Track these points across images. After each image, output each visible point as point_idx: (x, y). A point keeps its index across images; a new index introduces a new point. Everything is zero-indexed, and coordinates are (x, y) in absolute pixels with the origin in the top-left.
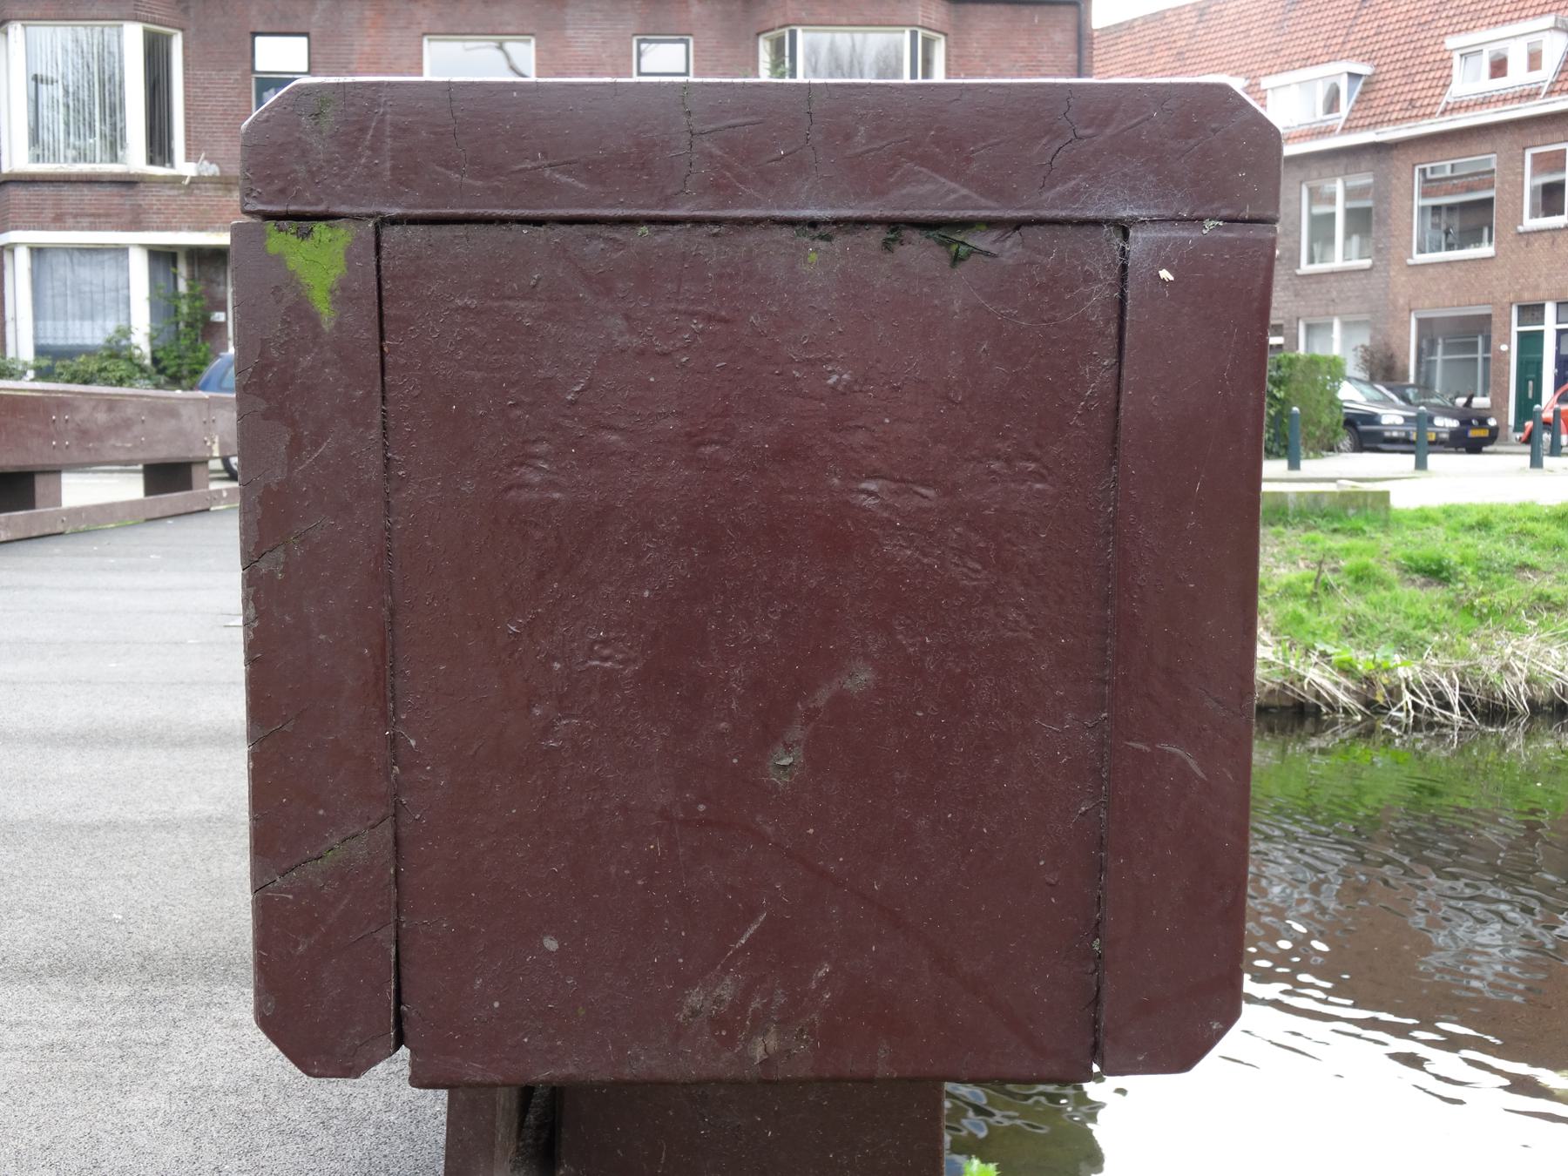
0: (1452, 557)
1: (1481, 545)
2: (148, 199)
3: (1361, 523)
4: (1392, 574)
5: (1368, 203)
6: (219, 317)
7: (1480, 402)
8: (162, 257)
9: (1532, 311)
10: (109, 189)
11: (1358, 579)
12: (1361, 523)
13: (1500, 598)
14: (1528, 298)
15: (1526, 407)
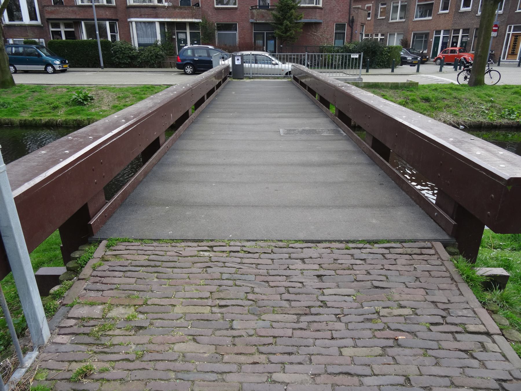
0: (431, 97)
1: (436, 94)
2: (159, 11)
3: (413, 89)
4: (419, 100)
5: (406, 3)
6: (174, 37)
7: (425, 52)
8: (162, 24)
9: (438, 32)
10: (150, 9)
11: (413, 101)
12: (413, 89)
13: (439, 105)
14: (438, 29)
15: (435, 53)
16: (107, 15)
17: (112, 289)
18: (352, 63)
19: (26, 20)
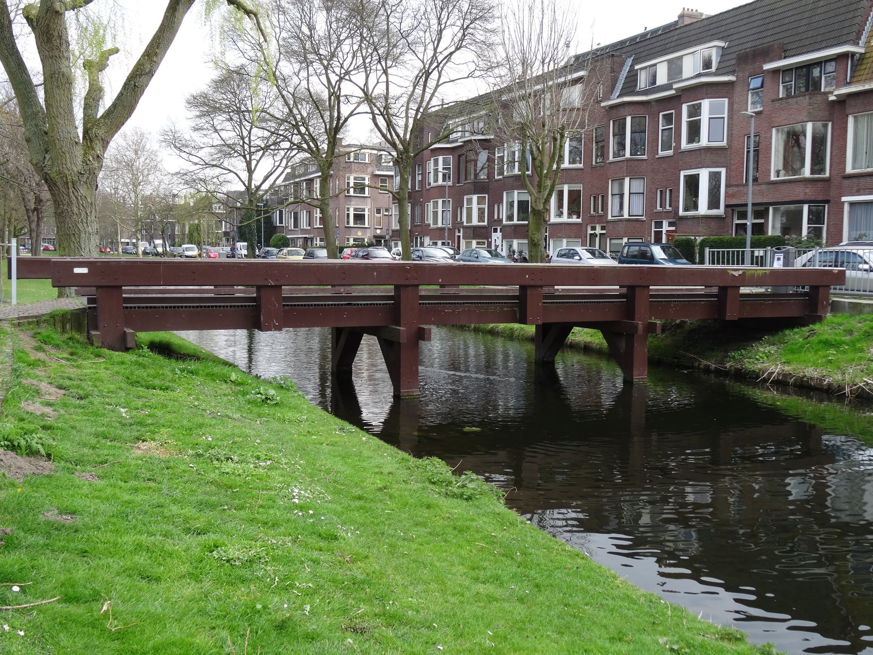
16: (806, 194)
17: (446, 49)
18: (733, 257)
19: (703, 208)
